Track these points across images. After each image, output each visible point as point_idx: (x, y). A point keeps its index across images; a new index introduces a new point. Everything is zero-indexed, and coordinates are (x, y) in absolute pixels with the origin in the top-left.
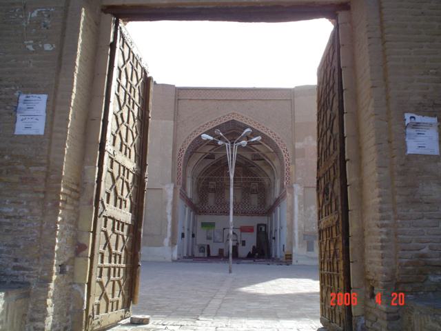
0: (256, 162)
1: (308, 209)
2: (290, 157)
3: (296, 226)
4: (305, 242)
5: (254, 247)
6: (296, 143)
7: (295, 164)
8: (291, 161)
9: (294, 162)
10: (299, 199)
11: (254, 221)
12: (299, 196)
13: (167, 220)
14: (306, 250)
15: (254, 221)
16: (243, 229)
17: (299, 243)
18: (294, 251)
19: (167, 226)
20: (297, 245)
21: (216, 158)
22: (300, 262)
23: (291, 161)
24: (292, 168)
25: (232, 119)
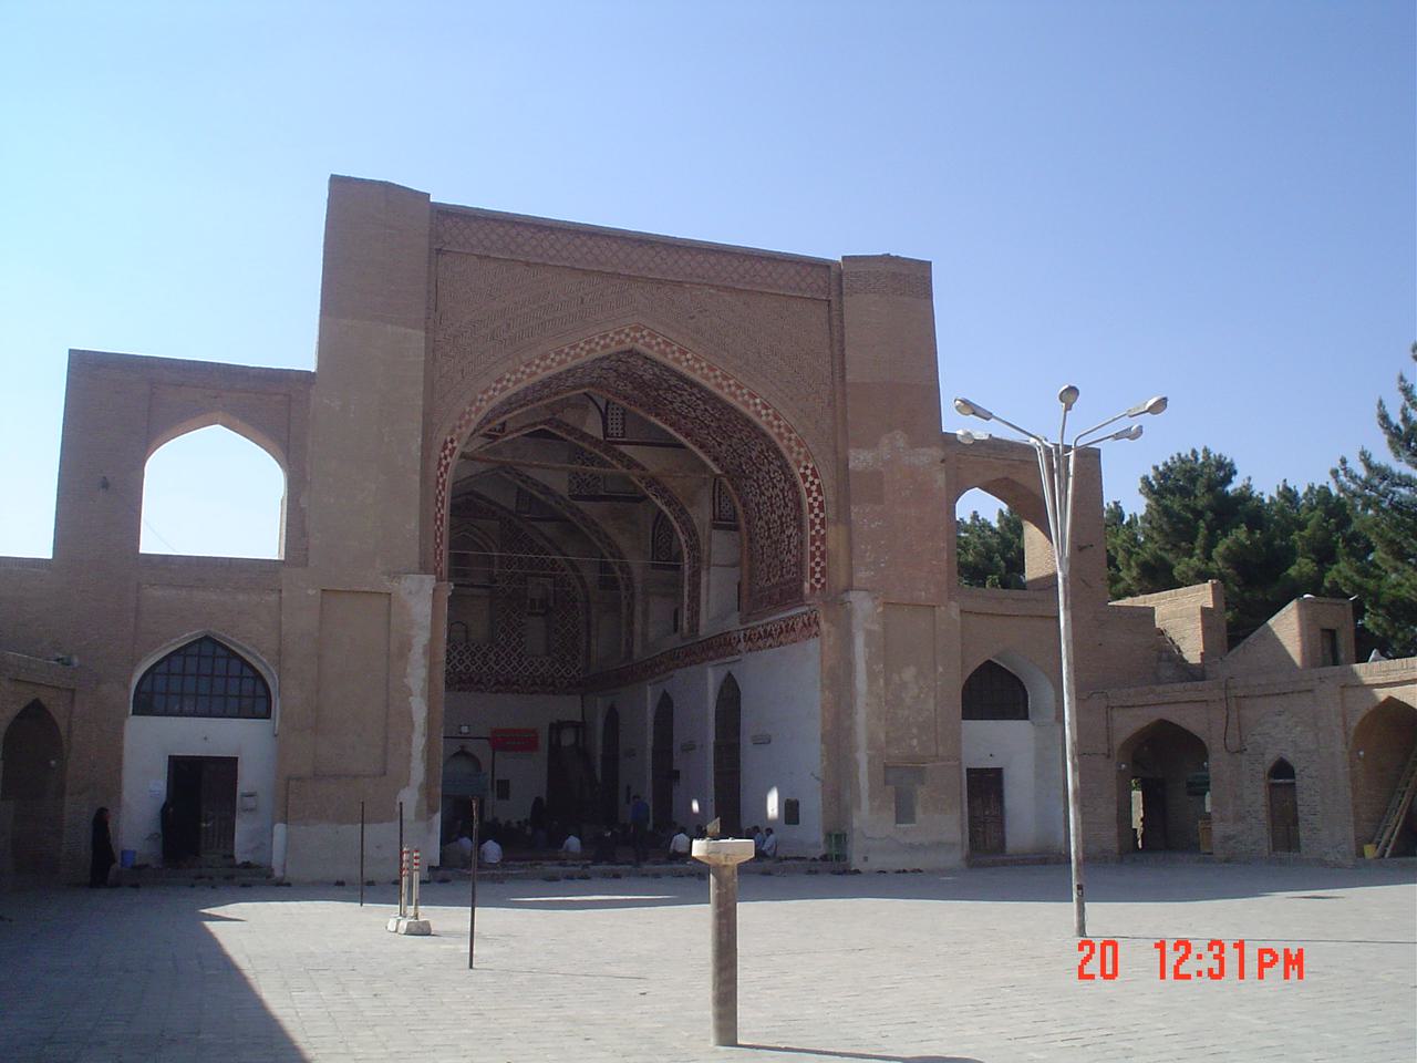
0: (581, 505)
1: (896, 677)
2: (829, 496)
3: (861, 737)
4: (890, 788)
5: (538, 800)
6: (852, 453)
7: (848, 523)
8: (830, 513)
9: (843, 517)
10: (867, 645)
11: (538, 712)
12: (869, 633)
13: (407, 716)
14: (893, 815)
15: (538, 712)
16: (503, 741)
17: (872, 796)
18: (856, 823)
19: (409, 741)
20: (865, 803)
22: (877, 862)
23: (830, 513)
24: (835, 537)
25: (628, 344)
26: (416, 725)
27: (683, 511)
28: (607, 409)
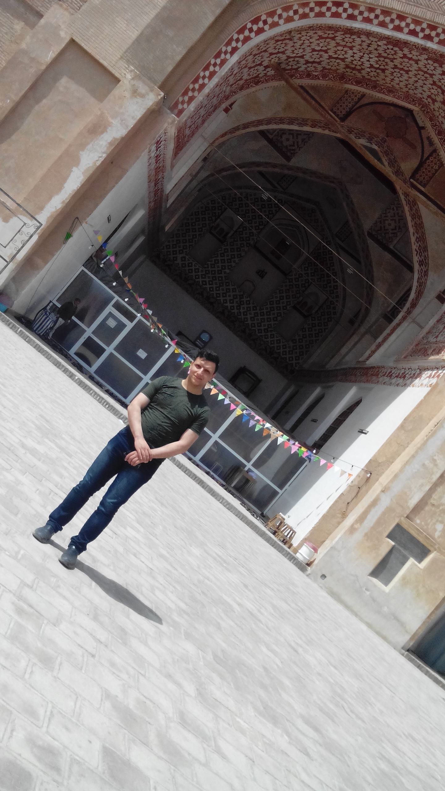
21: (294, 162)
26: (63, 191)
27: (426, 273)
28: (428, 158)
